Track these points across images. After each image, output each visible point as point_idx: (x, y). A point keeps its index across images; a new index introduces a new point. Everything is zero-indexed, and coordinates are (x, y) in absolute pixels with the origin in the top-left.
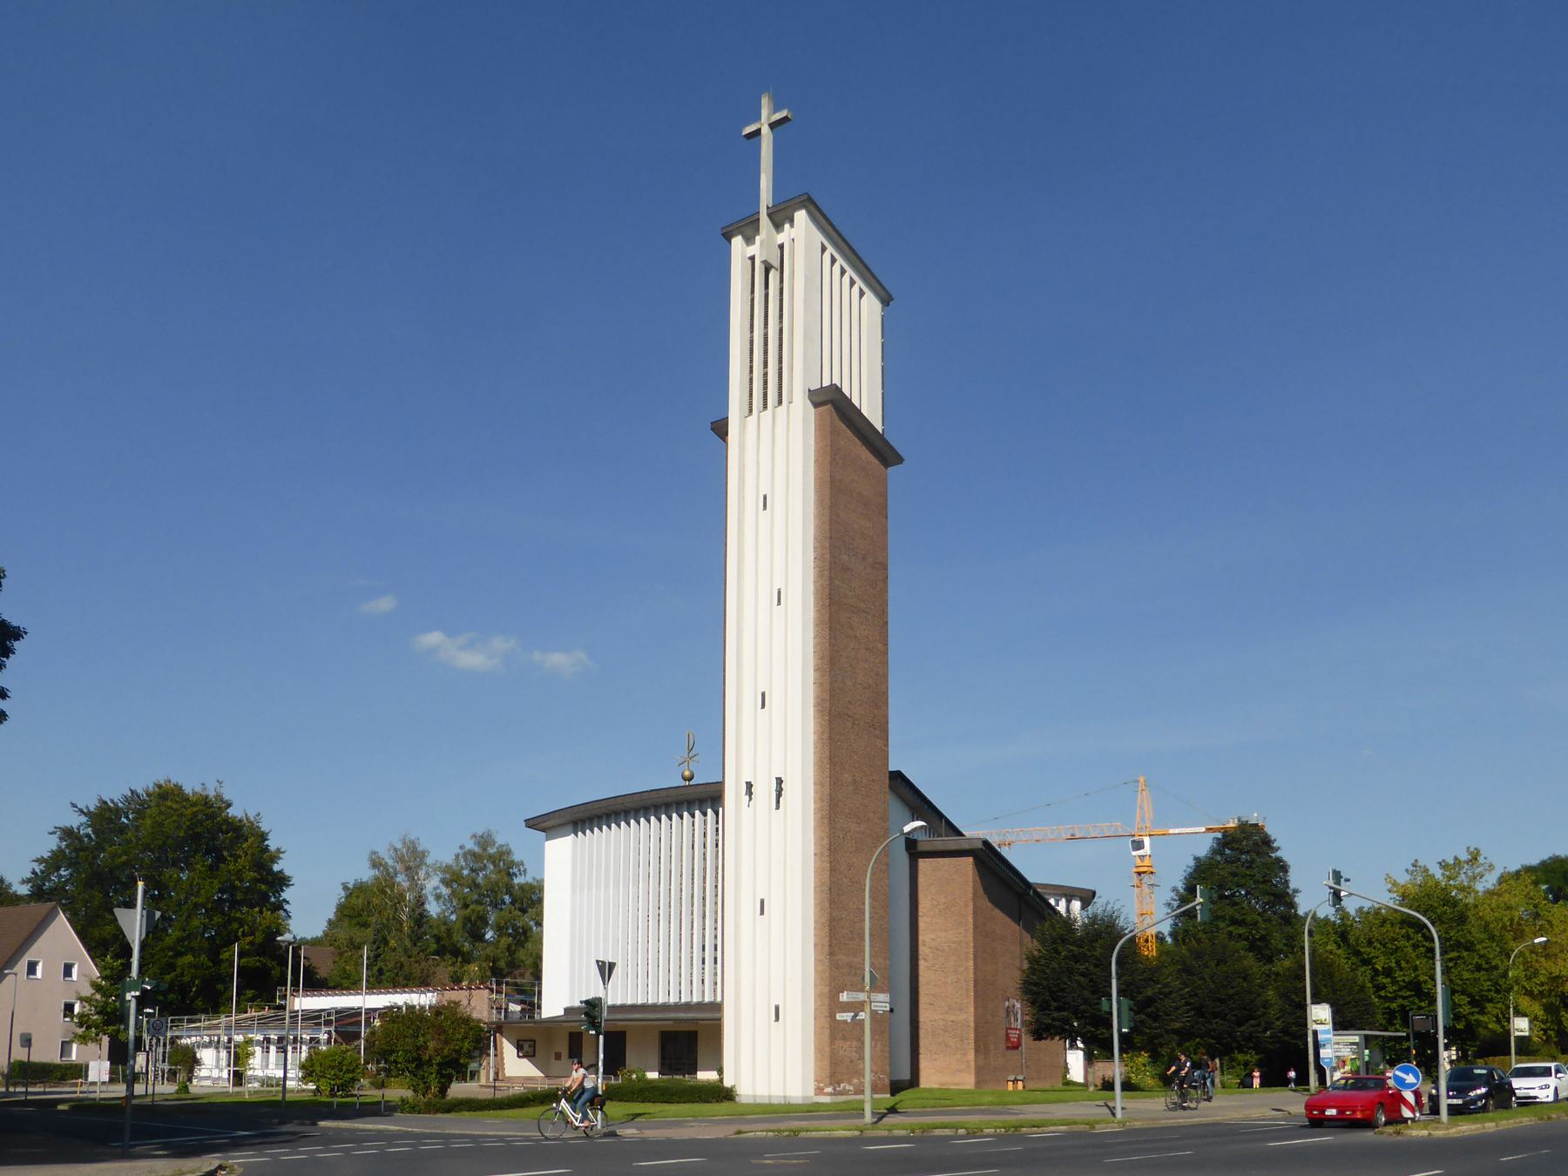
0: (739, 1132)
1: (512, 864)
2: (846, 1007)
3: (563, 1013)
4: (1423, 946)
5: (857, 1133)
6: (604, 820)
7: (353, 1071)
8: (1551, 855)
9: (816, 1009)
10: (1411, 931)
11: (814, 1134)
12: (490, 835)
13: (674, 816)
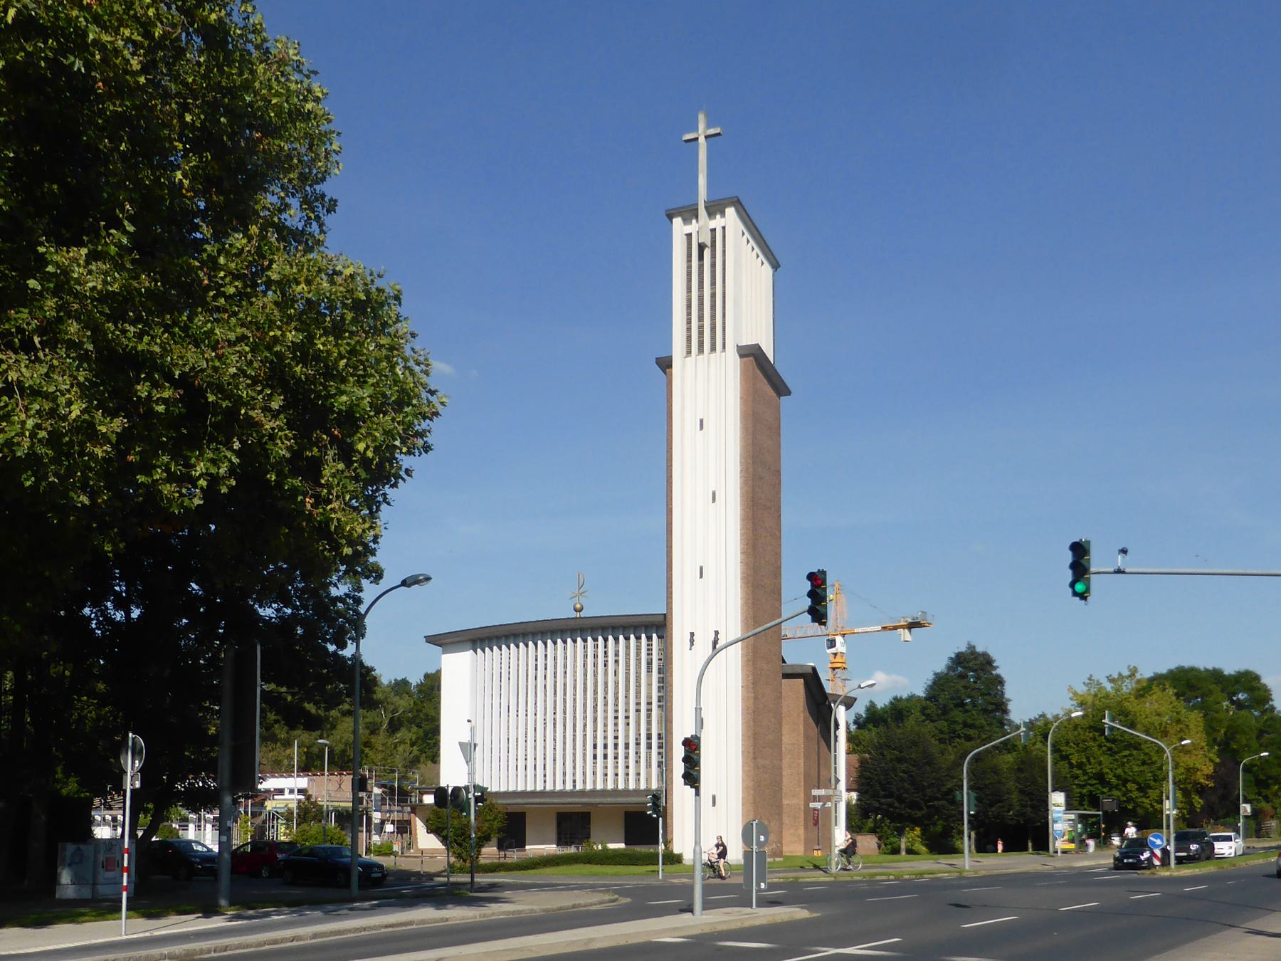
2: (815, 799)
4: (1105, 746)
8: (1177, 666)
10: (1097, 734)
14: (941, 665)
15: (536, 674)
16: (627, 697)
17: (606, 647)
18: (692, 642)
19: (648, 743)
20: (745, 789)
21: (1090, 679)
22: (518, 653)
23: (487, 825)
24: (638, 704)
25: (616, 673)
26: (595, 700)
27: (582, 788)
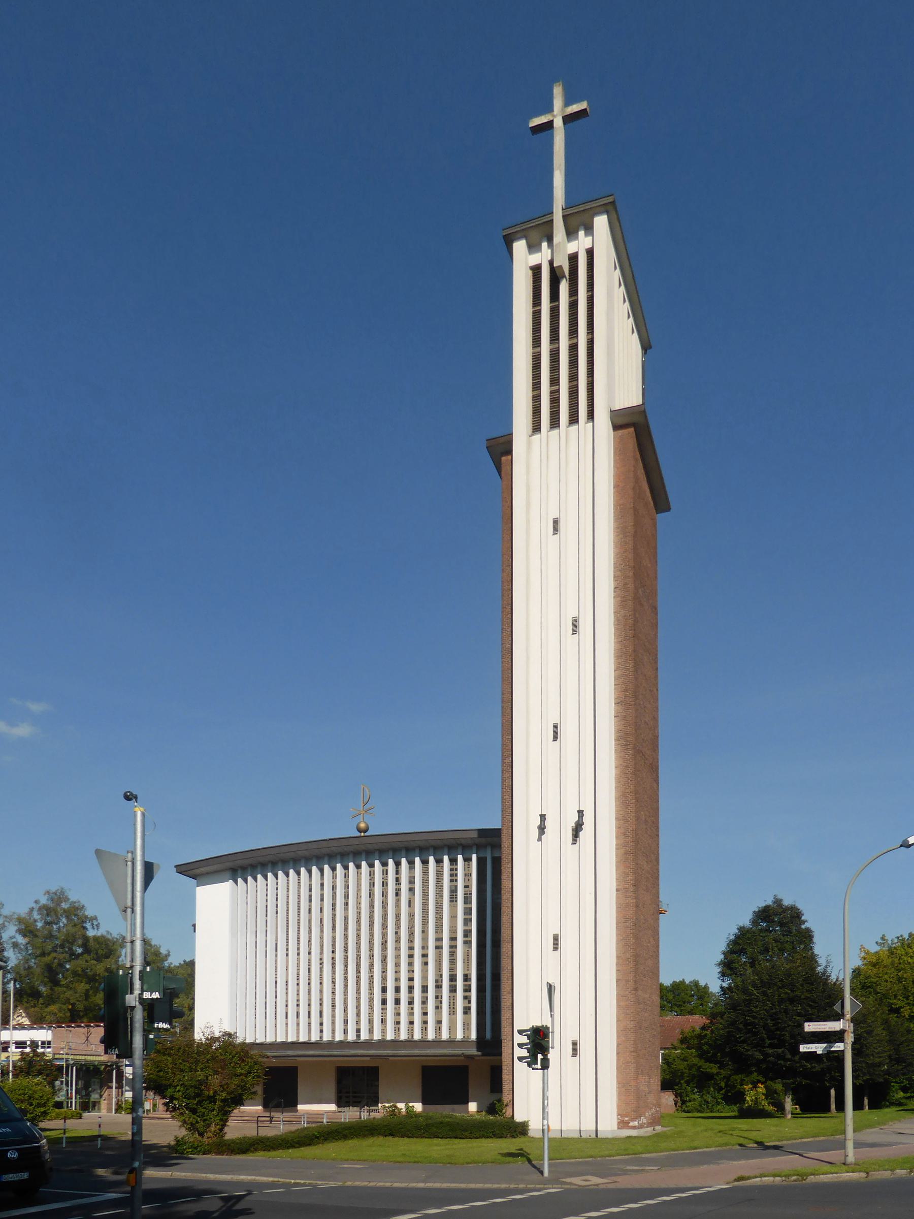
6: (249, 871)
7: (44, 1105)
9: (618, 1045)
12: (62, 892)
14: (746, 920)
15: (310, 906)
17: (397, 872)
18: (542, 829)
21: (883, 938)
22: (288, 883)
23: (236, 1081)
25: (410, 903)
26: (384, 935)
27: (367, 1038)
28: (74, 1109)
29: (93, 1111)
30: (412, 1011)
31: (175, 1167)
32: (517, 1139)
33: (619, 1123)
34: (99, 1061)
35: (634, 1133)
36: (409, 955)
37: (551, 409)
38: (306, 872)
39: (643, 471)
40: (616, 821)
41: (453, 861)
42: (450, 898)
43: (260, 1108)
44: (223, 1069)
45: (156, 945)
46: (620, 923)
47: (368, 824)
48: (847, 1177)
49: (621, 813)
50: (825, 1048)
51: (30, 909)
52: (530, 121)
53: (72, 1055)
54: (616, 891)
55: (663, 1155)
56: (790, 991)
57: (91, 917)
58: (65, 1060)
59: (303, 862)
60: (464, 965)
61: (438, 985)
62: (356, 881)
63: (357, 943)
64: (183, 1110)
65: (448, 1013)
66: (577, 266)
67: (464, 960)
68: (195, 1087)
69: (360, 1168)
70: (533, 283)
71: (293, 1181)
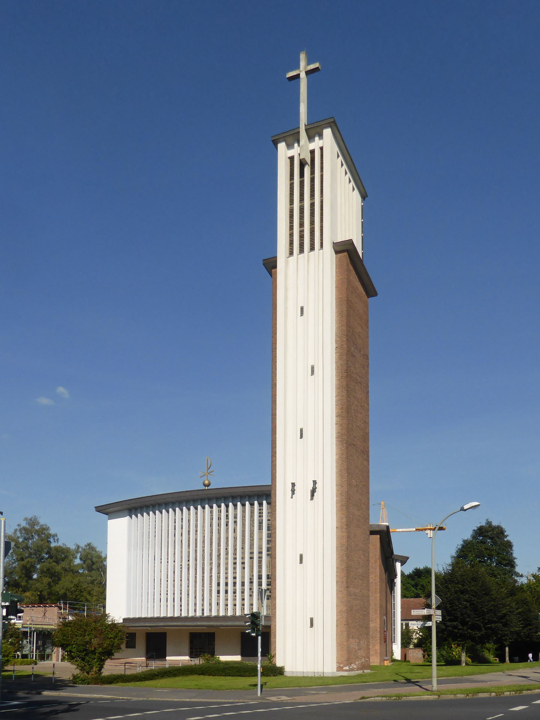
0: (363, 698)
1: (49, 536)
3: (122, 622)
5: (436, 697)
7: (7, 656)
9: (337, 620)
11: (411, 698)
12: (36, 519)
13: (164, 511)
14: (468, 535)
16: (243, 548)
17: (227, 511)
18: (293, 491)
19: (259, 582)
20: (339, 612)
23: (108, 642)
24: (252, 553)
25: (235, 531)
26: (219, 550)
28: (34, 659)
29: (47, 660)
30: (235, 598)
31: (62, 690)
32: (276, 677)
33: (337, 667)
34: (51, 629)
35: (345, 674)
36: (234, 563)
37: (300, 241)
38: (173, 511)
39: (355, 276)
40: (336, 486)
41: (261, 504)
42: (259, 527)
43: (144, 658)
44: (100, 635)
45: (99, 551)
46: (339, 547)
47: (211, 482)
48: (426, 698)
49: (339, 481)
50: (422, 624)
51: (15, 530)
52: (287, 74)
53: (34, 624)
54: (336, 528)
55: (341, 686)
56: (461, 586)
57: (53, 534)
58: (29, 628)
59: (170, 505)
60: (267, 569)
61: (252, 582)
62: (203, 517)
63: (203, 555)
64: (77, 658)
65: (257, 599)
66: (314, 157)
67: (267, 566)
68: (83, 645)
69: (167, 691)
70: (290, 167)
71: (121, 698)
